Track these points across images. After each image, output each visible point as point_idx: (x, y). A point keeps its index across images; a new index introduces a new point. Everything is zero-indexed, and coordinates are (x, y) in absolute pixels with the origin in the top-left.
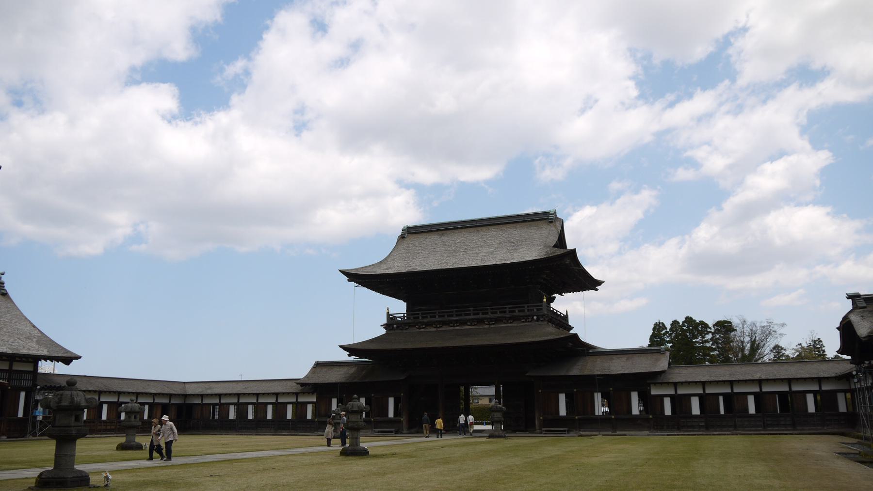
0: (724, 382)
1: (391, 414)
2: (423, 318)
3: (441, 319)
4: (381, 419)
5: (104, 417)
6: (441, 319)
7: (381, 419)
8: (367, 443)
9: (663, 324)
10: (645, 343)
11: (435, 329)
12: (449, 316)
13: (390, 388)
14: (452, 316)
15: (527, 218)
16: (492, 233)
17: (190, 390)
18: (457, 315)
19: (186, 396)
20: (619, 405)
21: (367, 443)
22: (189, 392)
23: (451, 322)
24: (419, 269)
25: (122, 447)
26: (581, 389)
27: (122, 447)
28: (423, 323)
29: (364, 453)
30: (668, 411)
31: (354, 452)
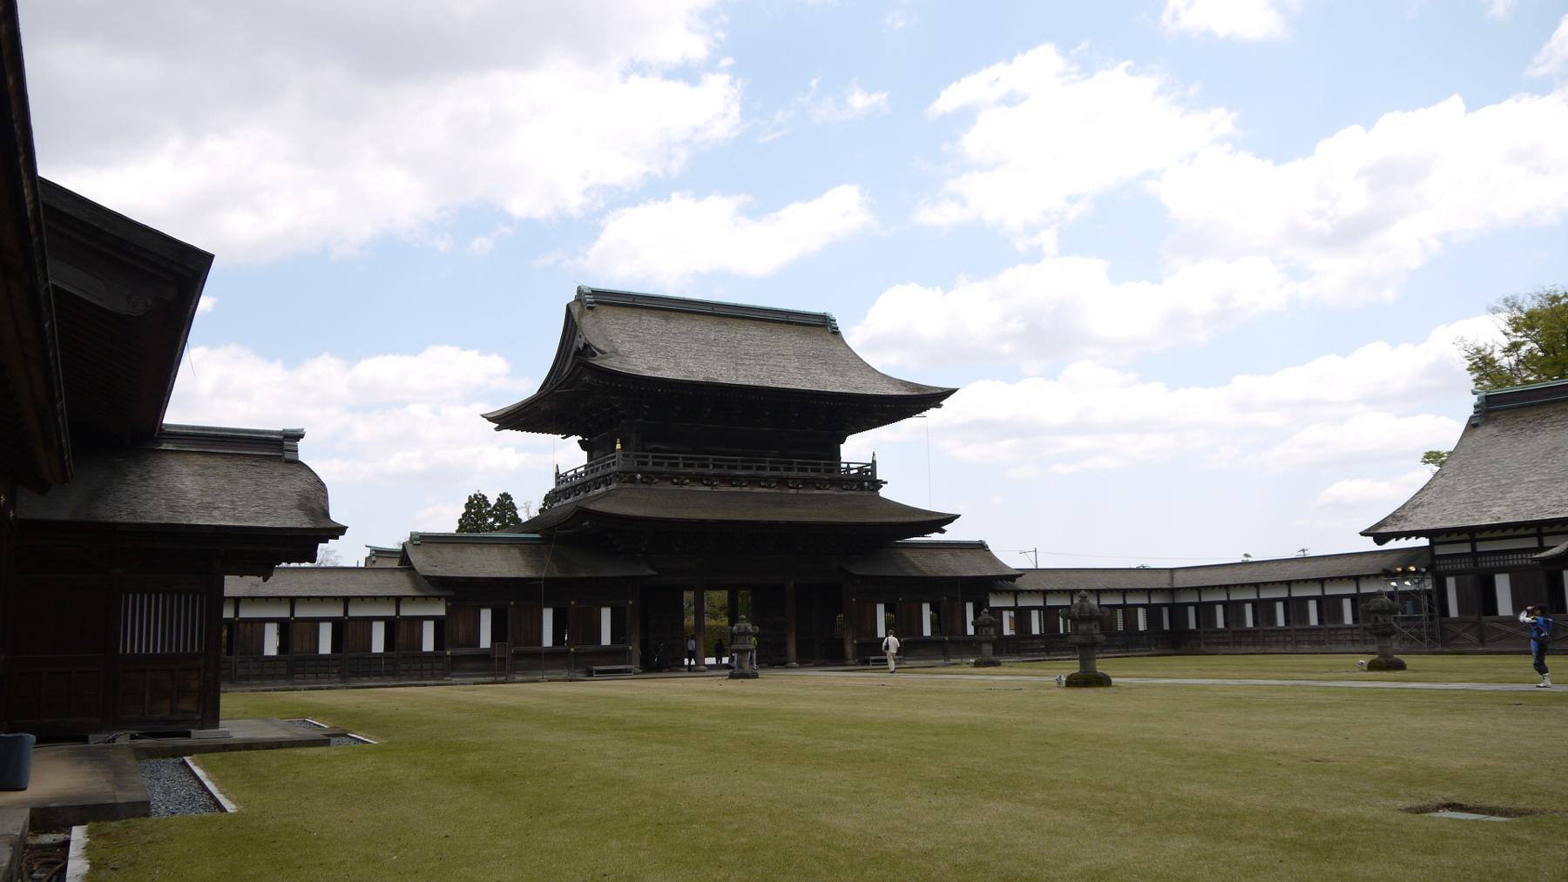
0: (388, 598)
1: (606, 639)
2: (686, 465)
3: (717, 471)
4: (591, 648)
5: (1036, 630)
6: (717, 471)
7: (591, 648)
8: (1102, 666)
9: (484, 497)
10: (451, 527)
11: (707, 489)
12: (729, 467)
13: (602, 591)
14: (735, 468)
15: (791, 319)
16: (699, 327)
17: (1180, 581)
18: (744, 468)
19: (1172, 591)
20: (947, 620)
21: (1102, 666)
22: (1179, 583)
23: (737, 478)
24: (722, 380)
25: (1073, 682)
26: (907, 593)
27: (1073, 682)
28: (688, 475)
29: (1104, 682)
30: (378, 646)
31: (1088, 680)
